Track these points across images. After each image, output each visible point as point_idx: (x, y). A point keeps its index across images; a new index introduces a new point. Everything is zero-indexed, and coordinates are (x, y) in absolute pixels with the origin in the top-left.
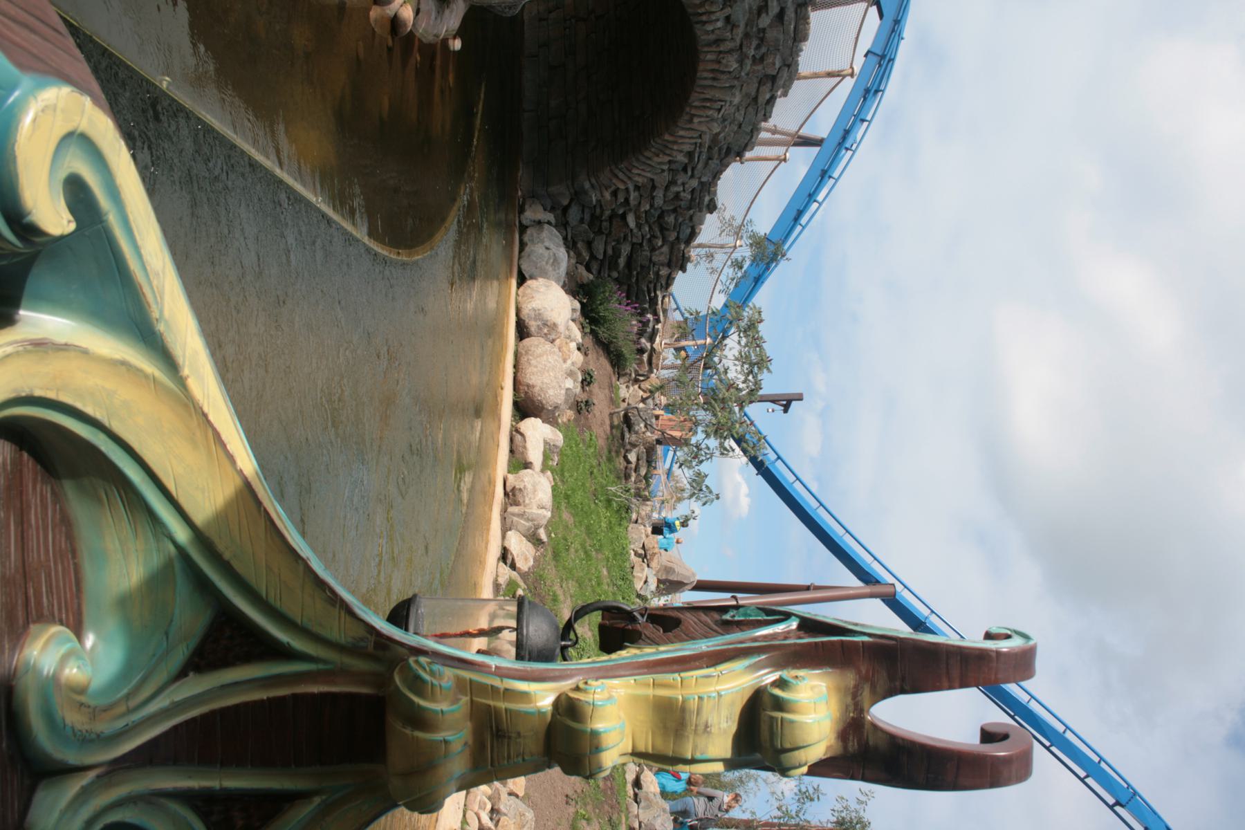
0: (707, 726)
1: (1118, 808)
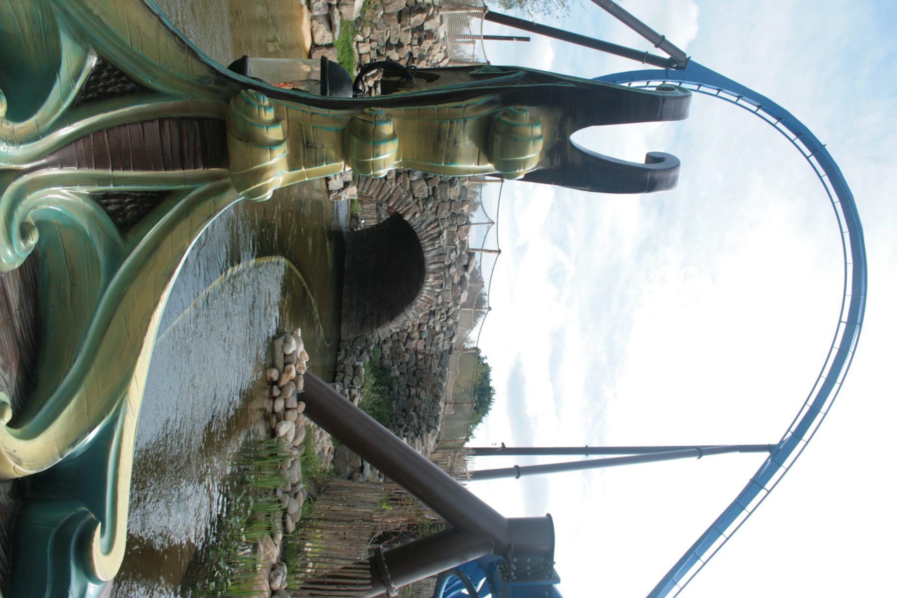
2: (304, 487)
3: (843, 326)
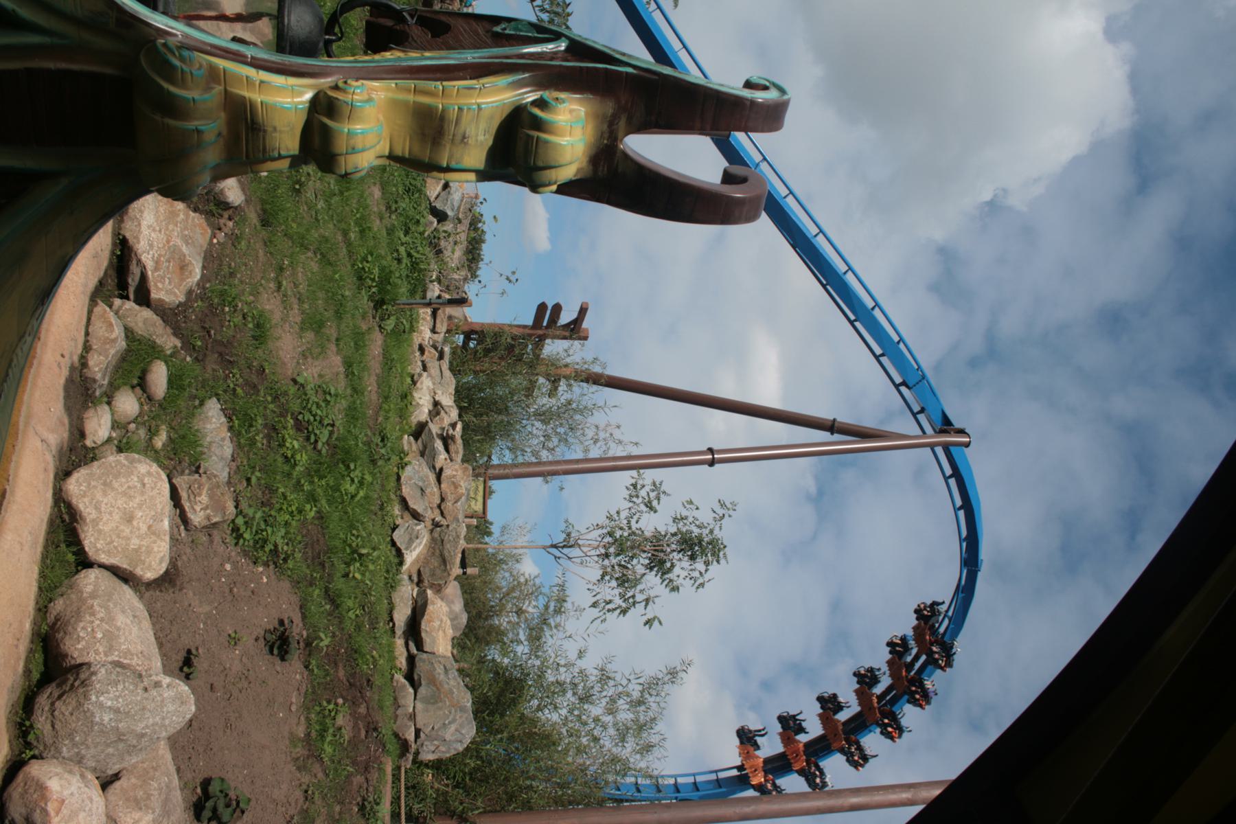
0: (464, 137)
1: (903, 389)
2: (509, 402)
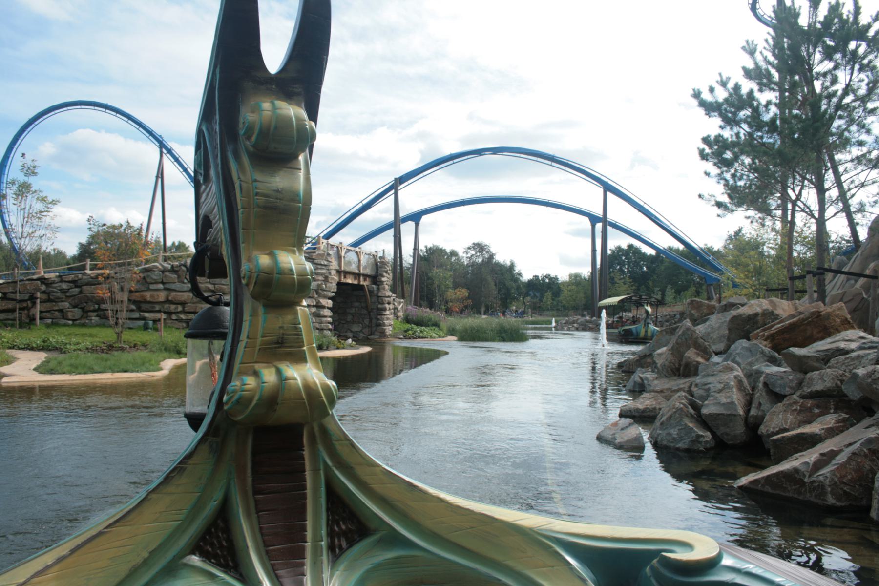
3: (554, 164)
